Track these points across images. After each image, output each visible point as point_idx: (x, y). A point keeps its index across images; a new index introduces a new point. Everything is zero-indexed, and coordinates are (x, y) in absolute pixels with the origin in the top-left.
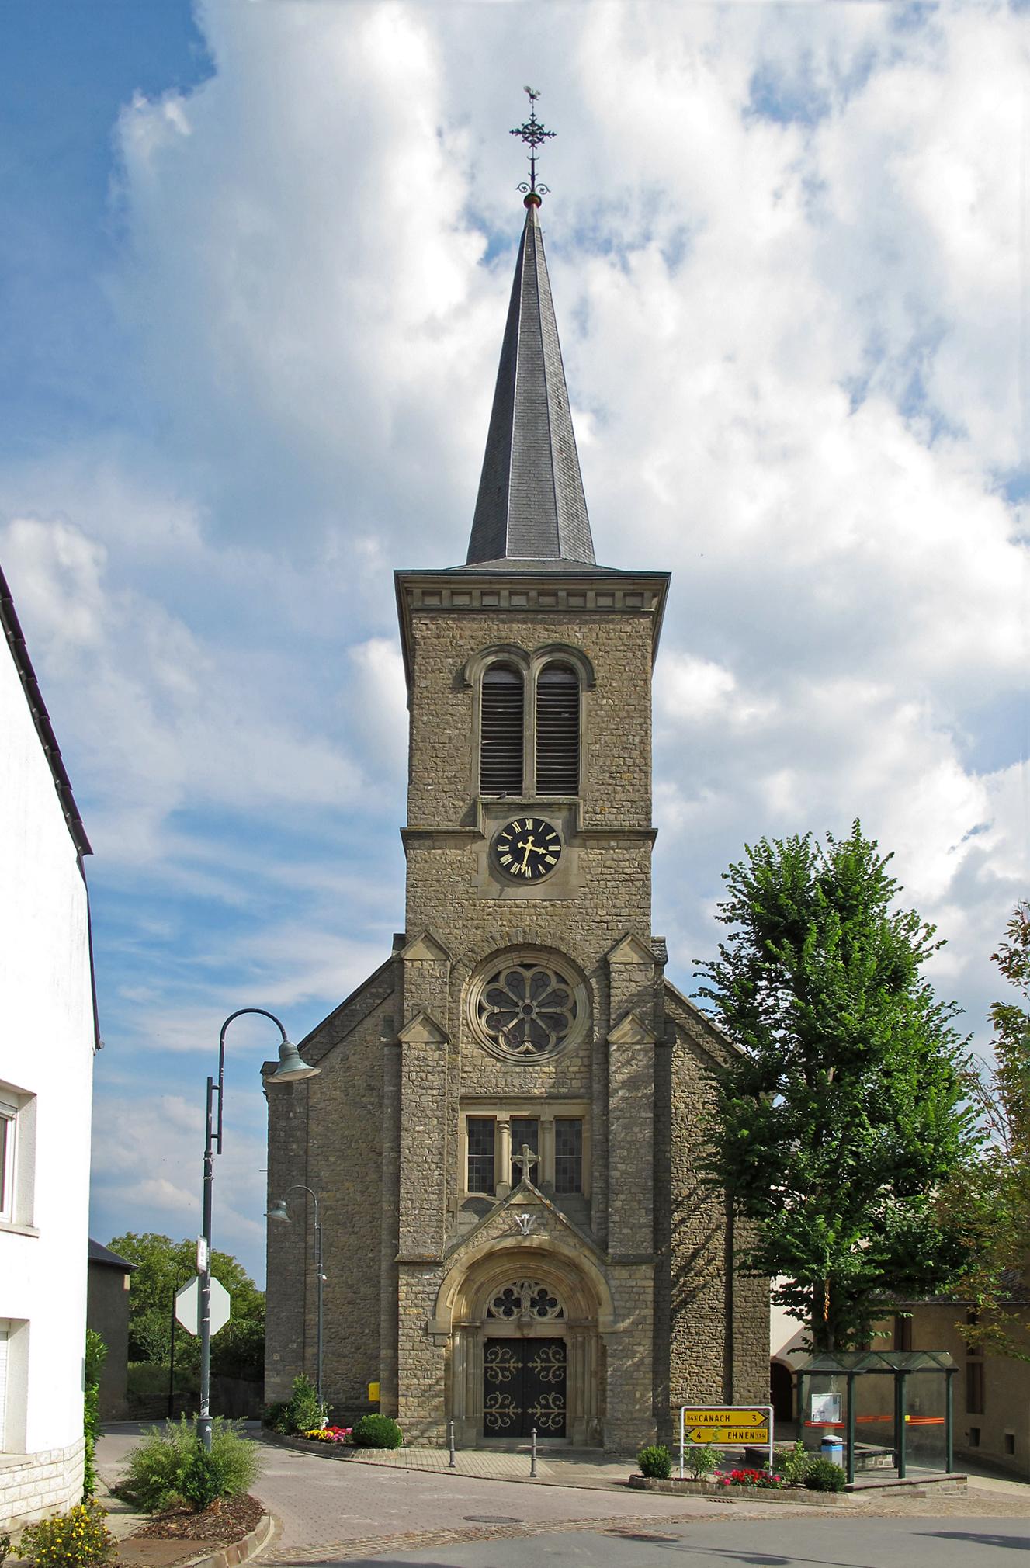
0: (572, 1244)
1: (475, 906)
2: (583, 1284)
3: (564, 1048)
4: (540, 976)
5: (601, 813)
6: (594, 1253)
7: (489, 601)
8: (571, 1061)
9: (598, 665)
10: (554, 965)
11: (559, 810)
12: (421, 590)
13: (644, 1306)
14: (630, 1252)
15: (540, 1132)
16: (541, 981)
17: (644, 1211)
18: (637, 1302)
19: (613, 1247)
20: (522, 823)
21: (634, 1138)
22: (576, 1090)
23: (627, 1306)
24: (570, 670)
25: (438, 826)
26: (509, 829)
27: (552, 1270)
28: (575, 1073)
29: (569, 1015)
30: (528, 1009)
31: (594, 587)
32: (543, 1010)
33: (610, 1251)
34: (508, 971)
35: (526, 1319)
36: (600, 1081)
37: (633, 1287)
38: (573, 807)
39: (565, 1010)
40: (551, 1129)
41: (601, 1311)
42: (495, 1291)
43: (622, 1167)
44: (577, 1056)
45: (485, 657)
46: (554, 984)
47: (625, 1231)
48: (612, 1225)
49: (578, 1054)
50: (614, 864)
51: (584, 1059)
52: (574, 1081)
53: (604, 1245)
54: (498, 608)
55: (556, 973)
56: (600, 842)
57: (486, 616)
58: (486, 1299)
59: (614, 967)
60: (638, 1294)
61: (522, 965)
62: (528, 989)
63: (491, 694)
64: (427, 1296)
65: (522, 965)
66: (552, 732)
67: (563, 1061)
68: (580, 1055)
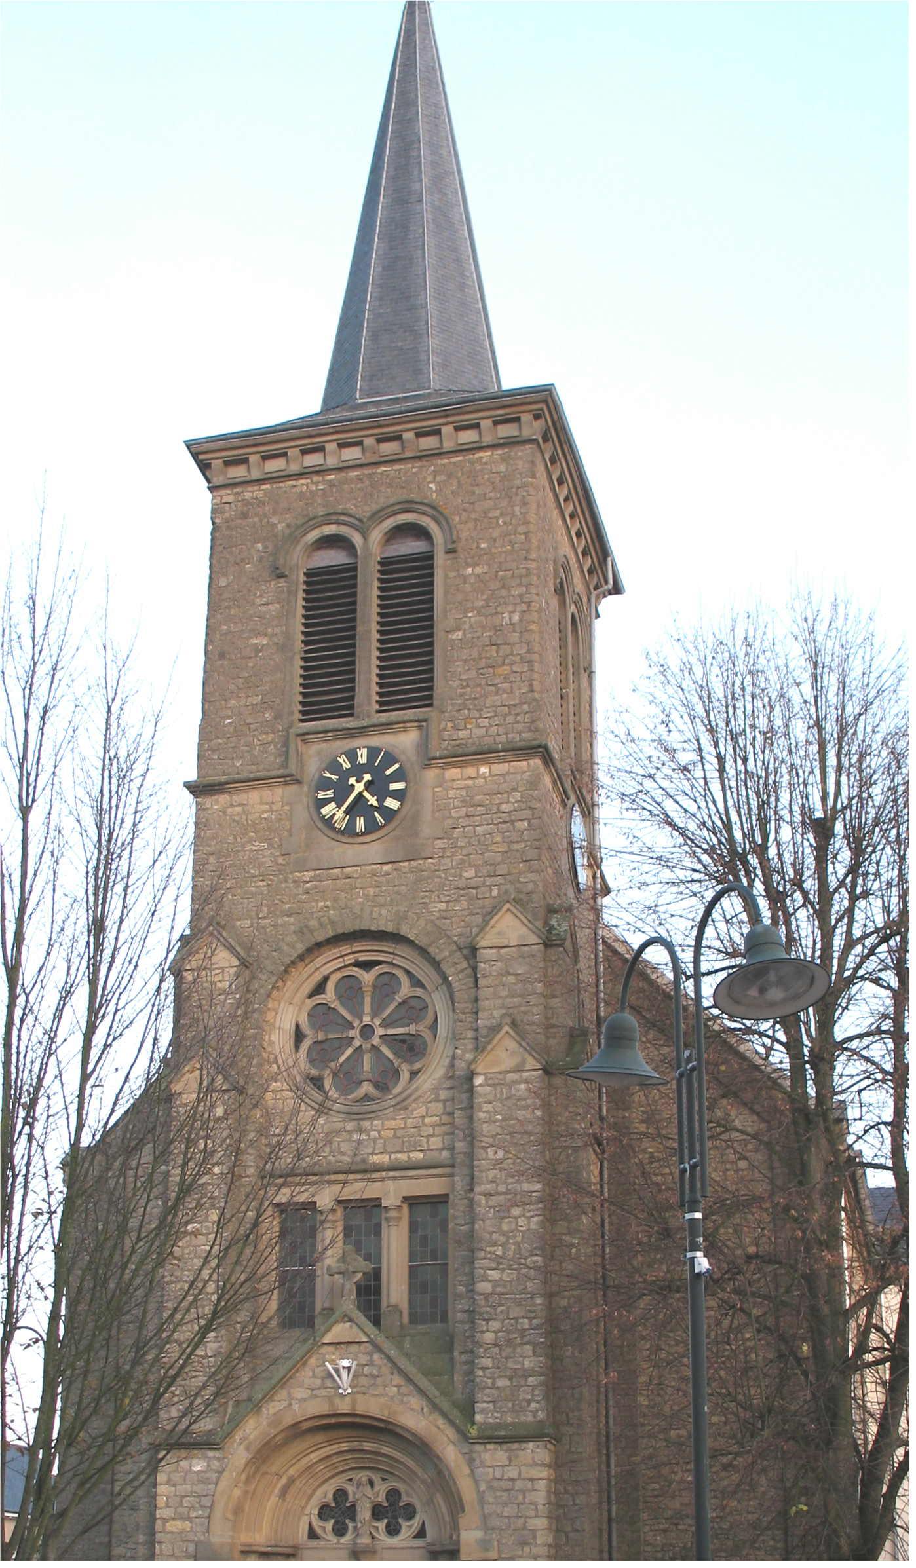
0: (418, 1408)
1: (286, 881)
2: (443, 1481)
3: (417, 1089)
4: (386, 978)
5: (466, 728)
6: (452, 1423)
7: (312, 460)
8: (427, 1109)
9: (461, 522)
10: (404, 958)
11: (405, 730)
12: (221, 461)
13: (532, 1513)
14: (509, 1420)
15: (384, 1224)
16: (387, 985)
17: (529, 1347)
18: (521, 1507)
19: (482, 1411)
20: (352, 755)
21: (514, 1226)
22: (435, 1154)
23: (505, 1514)
24: (421, 533)
25: (238, 774)
26: (334, 767)
27: (385, 1450)
28: (433, 1126)
29: (427, 1035)
30: (367, 1031)
31: (450, 419)
32: (391, 1031)
33: (478, 1418)
34: (339, 975)
35: (365, 1540)
36: (465, 1138)
37: (513, 1480)
38: (424, 724)
39: (421, 1028)
40: (399, 1218)
41: (463, 1521)
42: (319, 1493)
43: (494, 1275)
44: (437, 1100)
45: (305, 535)
46: (405, 989)
47: (501, 1383)
48: (480, 1373)
49: (438, 1095)
50: (486, 800)
51: (447, 1103)
52: (432, 1140)
53: (468, 1409)
54: (324, 467)
55: (408, 972)
56: (465, 770)
57: (309, 481)
58: (303, 1508)
59: (485, 954)
60: (523, 1492)
61: (357, 964)
62: (367, 1000)
63: (317, 583)
64: (198, 1500)
65: (357, 964)
66: (332, 614)
67: (415, 1110)
68: (442, 1097)
